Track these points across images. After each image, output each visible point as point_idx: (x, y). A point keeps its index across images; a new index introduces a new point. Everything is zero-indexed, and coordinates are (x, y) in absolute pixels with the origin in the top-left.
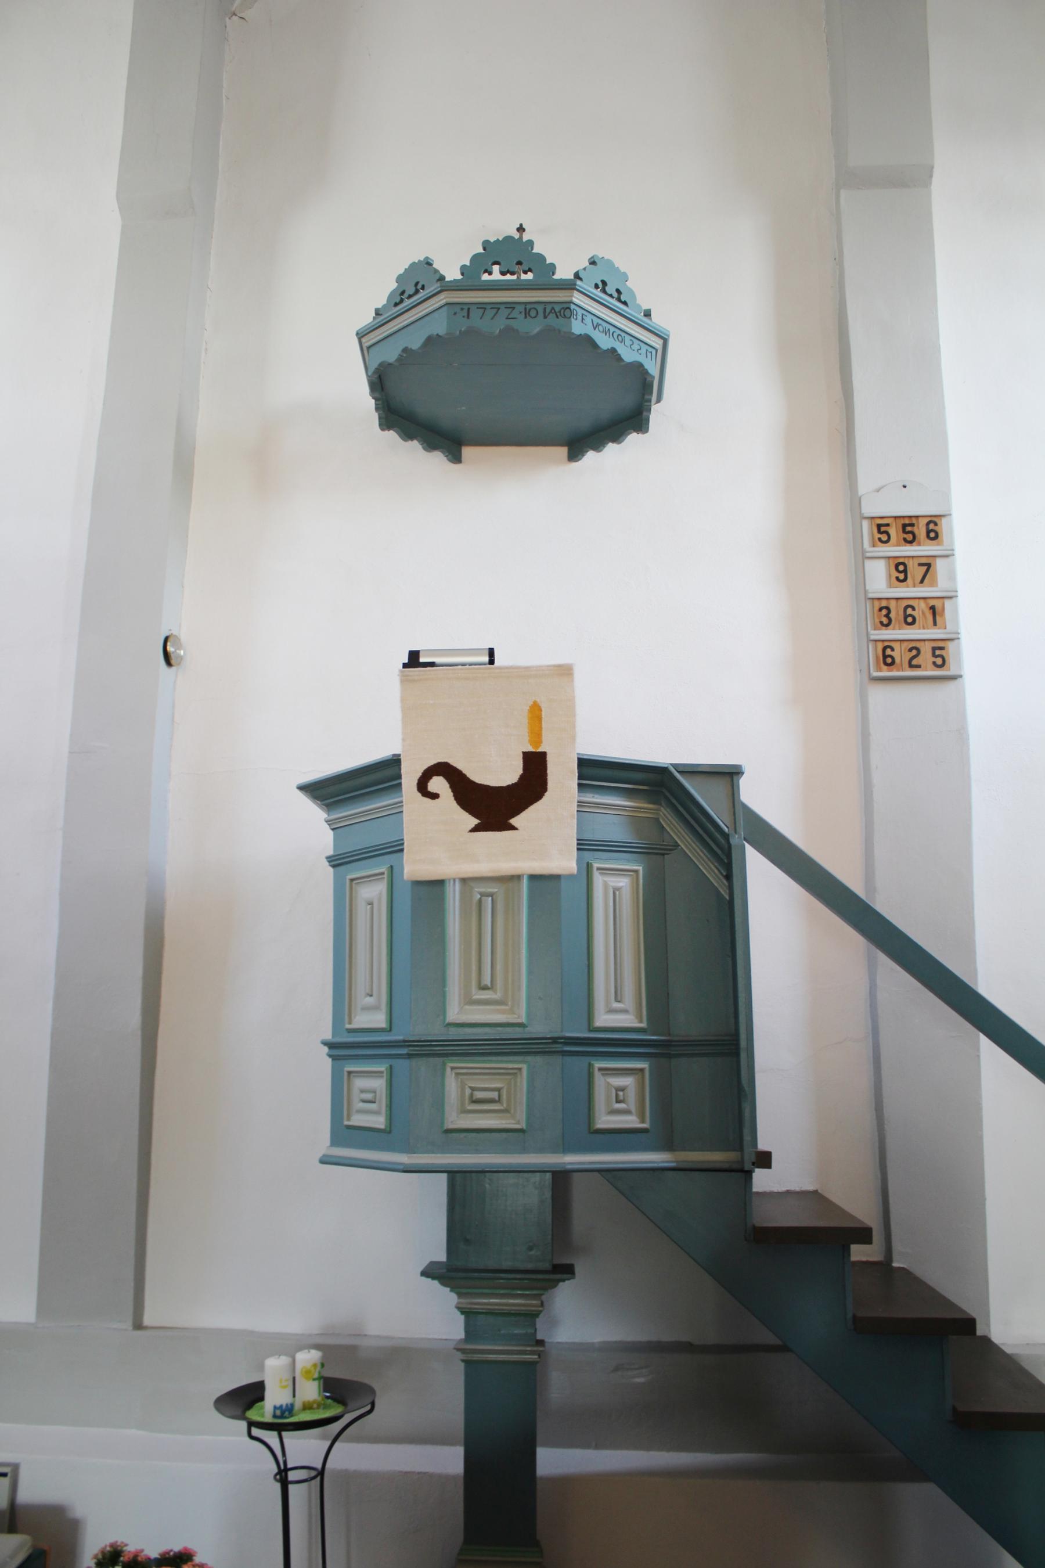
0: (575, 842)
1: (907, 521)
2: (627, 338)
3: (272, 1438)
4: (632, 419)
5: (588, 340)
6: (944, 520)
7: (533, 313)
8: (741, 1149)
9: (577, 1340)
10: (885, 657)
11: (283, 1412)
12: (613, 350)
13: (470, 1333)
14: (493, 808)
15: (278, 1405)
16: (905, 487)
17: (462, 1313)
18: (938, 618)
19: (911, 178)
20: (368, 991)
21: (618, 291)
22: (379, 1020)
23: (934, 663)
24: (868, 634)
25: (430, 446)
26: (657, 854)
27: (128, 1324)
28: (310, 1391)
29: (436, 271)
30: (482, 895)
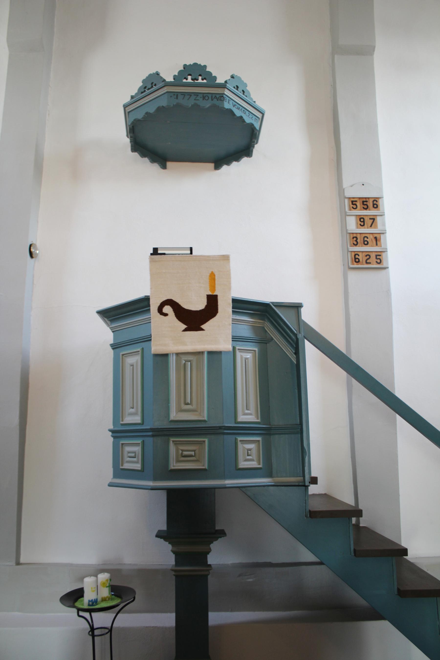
0: (231, 337)
1: (364, 200)
2: (247, 112)
3: (87, 615)
4: (246, 151)
5: (231, 112)
6: (380, 200)
7: (207, 98)
8: (304, 476)
9: (221, 563)
10: (355, 259)
11: (93, 603)
12: (241, 117)
13: (177, 563)
14: (193, 320)
15: (90, 600)
16: (363, 185)
17: (174, 553)
18: (378, 242)
19: (367, 51)
20: (131, 406)
21: (243, 91)
22: (137, 419)
23: (377, 262)
24: (348, 249)
25: (153, 160)
26: (263, 343)
27: (14, 563)
28: (105, 592)
29: (161, 78)
30: (186, 361)
